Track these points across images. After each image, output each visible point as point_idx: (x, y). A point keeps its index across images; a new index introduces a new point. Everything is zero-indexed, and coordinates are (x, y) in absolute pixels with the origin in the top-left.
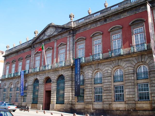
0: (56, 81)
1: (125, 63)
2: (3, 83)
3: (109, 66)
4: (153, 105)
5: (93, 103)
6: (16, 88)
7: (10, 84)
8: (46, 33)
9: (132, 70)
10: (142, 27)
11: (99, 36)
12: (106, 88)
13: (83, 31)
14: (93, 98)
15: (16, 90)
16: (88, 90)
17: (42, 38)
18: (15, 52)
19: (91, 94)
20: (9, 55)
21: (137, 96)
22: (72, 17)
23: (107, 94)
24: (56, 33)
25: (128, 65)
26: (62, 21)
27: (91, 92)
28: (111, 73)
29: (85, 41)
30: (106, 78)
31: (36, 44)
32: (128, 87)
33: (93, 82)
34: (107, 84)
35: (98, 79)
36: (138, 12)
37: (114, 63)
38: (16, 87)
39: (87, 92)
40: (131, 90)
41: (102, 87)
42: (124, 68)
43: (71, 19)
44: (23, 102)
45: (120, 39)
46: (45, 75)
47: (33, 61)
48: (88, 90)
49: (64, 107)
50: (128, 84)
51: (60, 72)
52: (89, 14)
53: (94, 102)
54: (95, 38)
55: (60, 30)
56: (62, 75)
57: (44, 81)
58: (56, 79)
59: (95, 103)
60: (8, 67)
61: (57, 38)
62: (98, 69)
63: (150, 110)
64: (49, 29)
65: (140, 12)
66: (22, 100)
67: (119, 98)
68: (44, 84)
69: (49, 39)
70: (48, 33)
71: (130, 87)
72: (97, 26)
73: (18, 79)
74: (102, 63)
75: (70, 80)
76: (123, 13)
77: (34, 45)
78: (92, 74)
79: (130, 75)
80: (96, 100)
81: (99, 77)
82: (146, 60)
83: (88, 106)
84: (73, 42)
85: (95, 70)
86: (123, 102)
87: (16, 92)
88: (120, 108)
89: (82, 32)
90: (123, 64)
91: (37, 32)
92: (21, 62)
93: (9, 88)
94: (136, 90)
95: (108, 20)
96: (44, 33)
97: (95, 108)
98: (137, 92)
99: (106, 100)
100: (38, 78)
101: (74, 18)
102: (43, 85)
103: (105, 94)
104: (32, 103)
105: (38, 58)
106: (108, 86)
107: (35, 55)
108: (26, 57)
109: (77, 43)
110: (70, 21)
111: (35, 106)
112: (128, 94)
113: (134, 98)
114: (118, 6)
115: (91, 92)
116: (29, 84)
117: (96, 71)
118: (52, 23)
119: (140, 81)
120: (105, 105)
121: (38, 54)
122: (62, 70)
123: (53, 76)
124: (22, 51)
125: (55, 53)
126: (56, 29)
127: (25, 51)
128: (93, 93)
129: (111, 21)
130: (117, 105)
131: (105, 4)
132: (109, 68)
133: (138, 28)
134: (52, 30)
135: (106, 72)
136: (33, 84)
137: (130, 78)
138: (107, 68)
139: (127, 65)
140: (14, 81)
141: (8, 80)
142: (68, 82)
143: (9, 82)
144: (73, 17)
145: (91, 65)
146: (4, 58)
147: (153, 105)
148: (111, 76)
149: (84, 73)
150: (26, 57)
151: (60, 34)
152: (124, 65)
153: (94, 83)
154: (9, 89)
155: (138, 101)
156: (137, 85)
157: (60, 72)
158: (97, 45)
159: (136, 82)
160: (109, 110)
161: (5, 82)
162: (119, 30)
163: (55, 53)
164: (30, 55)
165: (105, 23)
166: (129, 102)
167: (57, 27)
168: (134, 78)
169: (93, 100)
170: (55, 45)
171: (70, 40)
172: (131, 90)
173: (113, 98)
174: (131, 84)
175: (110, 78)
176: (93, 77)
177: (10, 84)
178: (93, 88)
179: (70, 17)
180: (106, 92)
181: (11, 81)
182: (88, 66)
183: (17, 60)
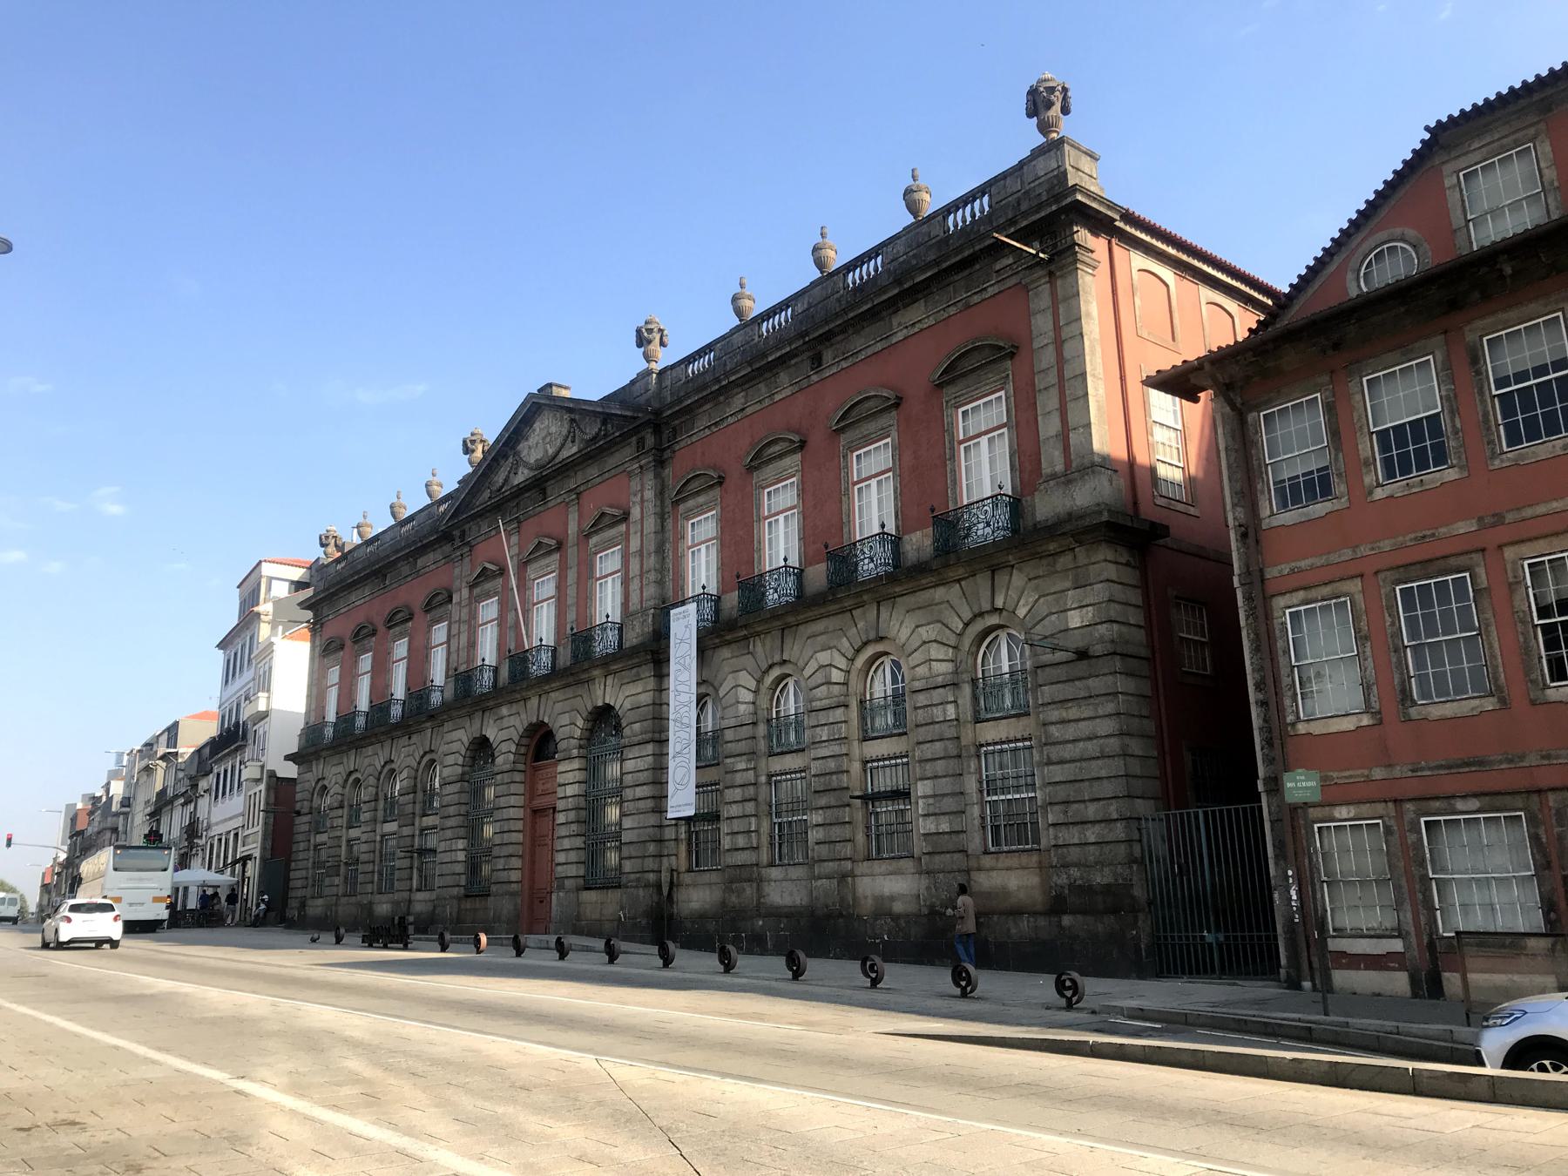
0: (581, 747)
1: (910, 623)
2: (308, 776)
3: (835, 643)
4: (1055, 878)
5: (763, 871)
6: (381, 804)
7: (346, 781)
8: (523, 447)
9: (944, 664)
10: (1002, 393)
11: (787, 461)
13: (707, 432)
14: (765, 840)
15: (380, 814)
16: (737, 794)
17: (506, 481)
18: (367, 577)
19: (753, 820)
20: (333, 594)
21: (977, 822)
22: (650, 342)
23: (829, 812)
24: (575, 449)
25: (926, 633)
26: (599, 371)
27: (752, 804)
28: (845, 684)
29: (717, 492)
30: (823, 718)
31: (473, 518)
32: (928, 766)
33: (762, 746)
35: (1001, 685)
36: (976, 299)
37: (861, 625)
38: (381, 795)
40: (945, 785)
41: (1030, 739)
42: (909, 649)
43: (648, 358)
44: (419, 890)
45: (1005, 430)
46: (523, 716)
47: (464, 627)
48: (737, 794)
50: (929, 751)
51: (600, 693)
52: (910, 219)
53: (772, 865)
54: (769, 471)
55: (592, 429)
56: (608, 708)
57: (523, 750)
58: (578, 733)
59: (775, 873)
60: (334, 675)
61: (580, 478)
62: (785, 662)
63: (1039, 907)
64: (537, 425)
65: (991, 291)
66: (411, 879)
67: (886, 845)
68: (521, 767)
69: (540, 484)
70: (535, 449)
71: (940, 766)
72: (777, 397)
73: (387, 744)
74: (801, 628)
75: (648, 736)
76: (906, 306)
77: (467, 527)
78: (756, 692)
79: (937, 695)
80: (996, 842)
81: (1006, 669)
82: (1015, 597)
84: (662, 502)
85: (771, 667)
86: (907, 865)
87: (378, 831)
88: (892, 898)
89: (702, 435)
90: (902, 626)
91: (661, 331)
92: (401, 635)
93: (342, 807)
94: (971, 785)
95: (828, 356)
96: (513, 448)
98: (975, 797)
99: (824, 851)
100: (491, 734)
101: (662, 344)
102: (518, 777)
103: (817, 818)
104: (462, 891)
105: (489, 610)
106: (832, 764)
107: (472, 587)
108: (429, 607)
109: (682, 508)
110: (643, 365)
111: (475, 910)
112: (932, 810)
113: (958, 832)
114: (986, 199)
115: (750, 807)
116: (447, 772)
117: (776, 672)
118: (550, 385)
119: (989, 732)
120: (819, 882)
121: (488, 586)
122: (610, 680)
123: (565, 719)
124: (405, 569)
125: (572, 576)
126: (572, 420)
127: (420, 562)
128: (765, 808)
129: (844, 364)
130: (880, 880)
131: (916, 196)
132: (836, 654)
133: (981, 402)
134: (553, 429)
135: (819, 678)
136: (463, 774)
137: (938, 713)
138: (824, 657)
139: (922, 630)
140: (367, 761)
141: (335, 760)
142: (635, 752)
143: (340, 769)
144: (1058, 106)
145: (746, 638)
146: (309, 614)
147: (1055, 878)
148: (847, 706)
149: (717, 690)
150: (429, 607)
151: (593, 454)
152: (904, 633)
153: (976, 712)
154: (340, 812)
155: (986, 852)
156: (979, 757)
157: (600, 693)
158: (778, 514)
159: (967, 737)
160: (841, 915)
161: (318, 769)
162: (884, 421)
163: (572, 576)
164: (796, 438)
165: (815, 378)
166: (937, 858)
167: (575, 411)
168: (958, 714)
169: (764, 857)
170: (573, 528)
171: (642, 491)
172: (945, 785)
173: (860, 837)
174: (946, 749)
175: (839, 714)
176: (763, 714)
177: (346, 781)
178: (763, 779)
179: (642, 341)
180: (823, 801)
181: (351, 761)
182: (734, 646)
183: (379, 622)
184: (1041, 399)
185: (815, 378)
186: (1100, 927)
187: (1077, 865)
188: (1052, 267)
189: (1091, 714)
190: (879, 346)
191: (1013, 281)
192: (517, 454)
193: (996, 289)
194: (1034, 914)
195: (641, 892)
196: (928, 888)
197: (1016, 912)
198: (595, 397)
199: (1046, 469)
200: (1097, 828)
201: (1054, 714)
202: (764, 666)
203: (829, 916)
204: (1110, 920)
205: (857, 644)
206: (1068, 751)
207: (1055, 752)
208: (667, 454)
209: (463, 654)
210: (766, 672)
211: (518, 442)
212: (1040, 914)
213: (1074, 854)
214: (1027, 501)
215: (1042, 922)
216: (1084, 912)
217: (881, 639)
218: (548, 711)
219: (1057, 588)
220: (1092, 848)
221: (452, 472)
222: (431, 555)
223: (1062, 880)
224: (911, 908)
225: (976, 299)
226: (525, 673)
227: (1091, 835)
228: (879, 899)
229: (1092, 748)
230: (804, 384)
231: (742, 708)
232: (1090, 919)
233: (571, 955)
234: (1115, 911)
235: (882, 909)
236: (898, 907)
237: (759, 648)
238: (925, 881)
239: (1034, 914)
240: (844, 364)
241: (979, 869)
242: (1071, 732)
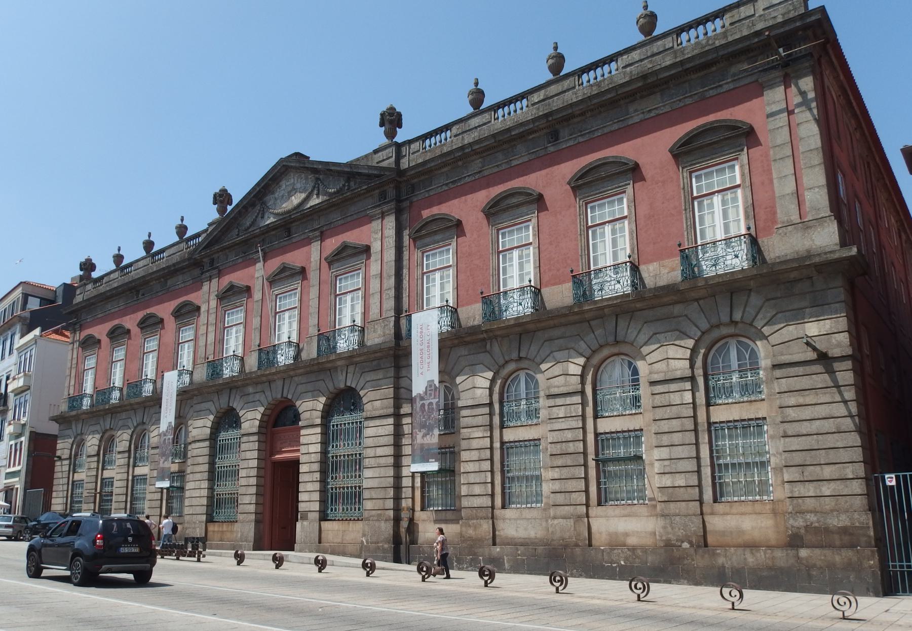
4: (791, 522)
12: (559, 446)
13: (445, 188)
17: (253, 223)
31: (223, 249)
34: (564, 426)
36: (712, 93)
39: (471, 464)
49: (364, 535)
63: (773, 542)
77: (215, 256)
83: (475, 528)
85: (507, 362)
88: (626, 534)
95: (564, 133)
97: (507, 538)
111: (222, 532)
120: (556, 522)
126: (318, 179)
127: (169, 282)
129: (581, 139)
137: (675, 398)
165: (552, 149)
166: (672, 505)
174: (682, 425)
184: (775, 167)
185: (552, 149)
186: (837, 558)
187: (814, 512)
188: (789, 70)
189: (830, 400)
190: (616, 127)
191: (753, 78)
192: (264, 203)
193: (731, 86)
194: (769, 547)
195: (383, 524)
196: (664, 528)
197: (752, 546)
198: (344, 160)
199: (781, 216)
200: (833, 485)
201: (792, 400)
202: (501, 362)
203: (566, 546)
204: (848, 554)
205: (595, 346)
206: (805, 428)
207: (791, 429)
208: (406, 204)
209: (211, 349)
210: (503, 366)
211: (265, 195)
212: (777, 547)
213: (810, 503)
214: (763, 241)
215: (779, 553)
216: (822, 547)
217: (617, 342)
218: (292, 391)
219: (796, 306)
220: (827, 499)
221: (202, 217)
222: (180, 278)
223: (800, 522)
224: (649, 541)
225: (712, 93)
226: (272, 362)
227: (827, 489)
228: (613, 535)
229: (829, 425)
230: (542, 153)
231: (479, 392)
232: (828, 552)
233: (376, 573)
234: (852, 546)
235: (616, 543)
236: (632, 541)
237: (496, 348)
238: (661, 522)
239: (769, 547)
240: (581, 139)
241: (712, 514)
242: (807, 413)
